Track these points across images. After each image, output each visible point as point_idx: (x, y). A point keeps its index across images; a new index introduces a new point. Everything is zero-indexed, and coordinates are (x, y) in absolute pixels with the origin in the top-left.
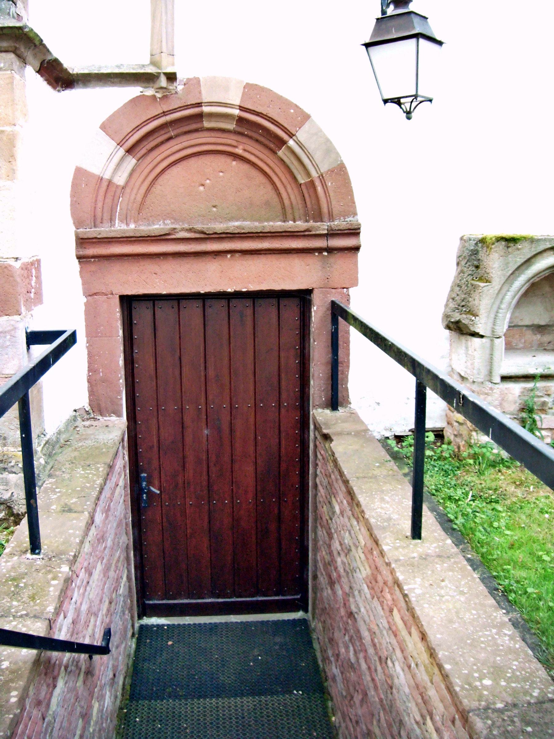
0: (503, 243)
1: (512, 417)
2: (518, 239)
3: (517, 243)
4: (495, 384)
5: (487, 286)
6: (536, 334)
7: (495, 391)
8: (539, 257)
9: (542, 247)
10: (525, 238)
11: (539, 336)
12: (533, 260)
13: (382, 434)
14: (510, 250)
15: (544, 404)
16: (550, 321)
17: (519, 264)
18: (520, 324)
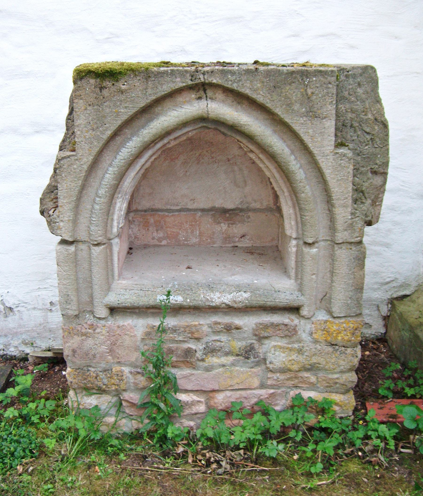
0: (92, 81)
1: (133, 370)
2: (120, 73)
3: (117, 81)
4: (100, 318)
5: (69, 157)
6: (219, 223)
7: (98, 330)
8: (168, 103)
9: (179, 83)
10: (132, 70)
11: (224, 226)
12: (158, 109)
13: (20, 349)
14: (105, 92)
15: (189, 352)
16: (242, 202)
17: (125, 117)
18: (190, 207)
